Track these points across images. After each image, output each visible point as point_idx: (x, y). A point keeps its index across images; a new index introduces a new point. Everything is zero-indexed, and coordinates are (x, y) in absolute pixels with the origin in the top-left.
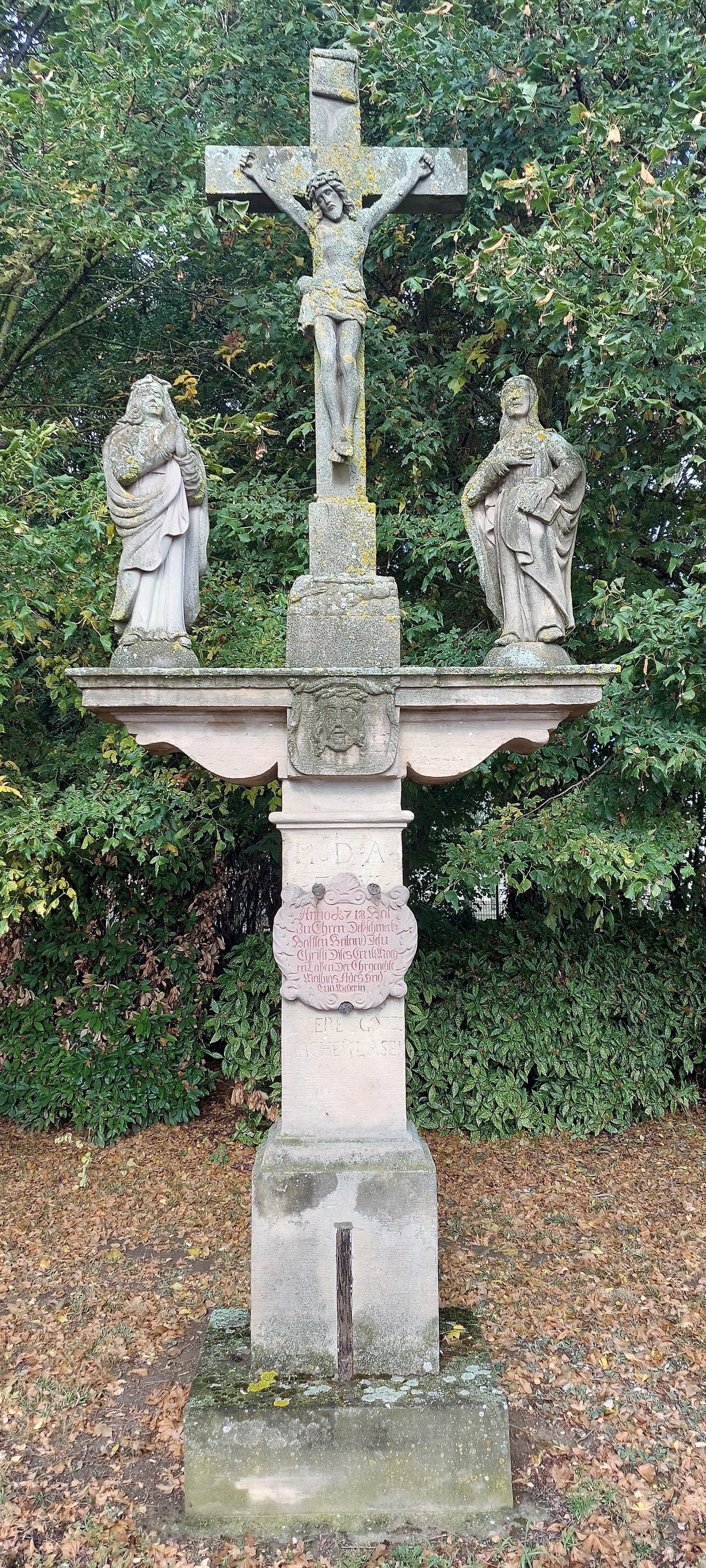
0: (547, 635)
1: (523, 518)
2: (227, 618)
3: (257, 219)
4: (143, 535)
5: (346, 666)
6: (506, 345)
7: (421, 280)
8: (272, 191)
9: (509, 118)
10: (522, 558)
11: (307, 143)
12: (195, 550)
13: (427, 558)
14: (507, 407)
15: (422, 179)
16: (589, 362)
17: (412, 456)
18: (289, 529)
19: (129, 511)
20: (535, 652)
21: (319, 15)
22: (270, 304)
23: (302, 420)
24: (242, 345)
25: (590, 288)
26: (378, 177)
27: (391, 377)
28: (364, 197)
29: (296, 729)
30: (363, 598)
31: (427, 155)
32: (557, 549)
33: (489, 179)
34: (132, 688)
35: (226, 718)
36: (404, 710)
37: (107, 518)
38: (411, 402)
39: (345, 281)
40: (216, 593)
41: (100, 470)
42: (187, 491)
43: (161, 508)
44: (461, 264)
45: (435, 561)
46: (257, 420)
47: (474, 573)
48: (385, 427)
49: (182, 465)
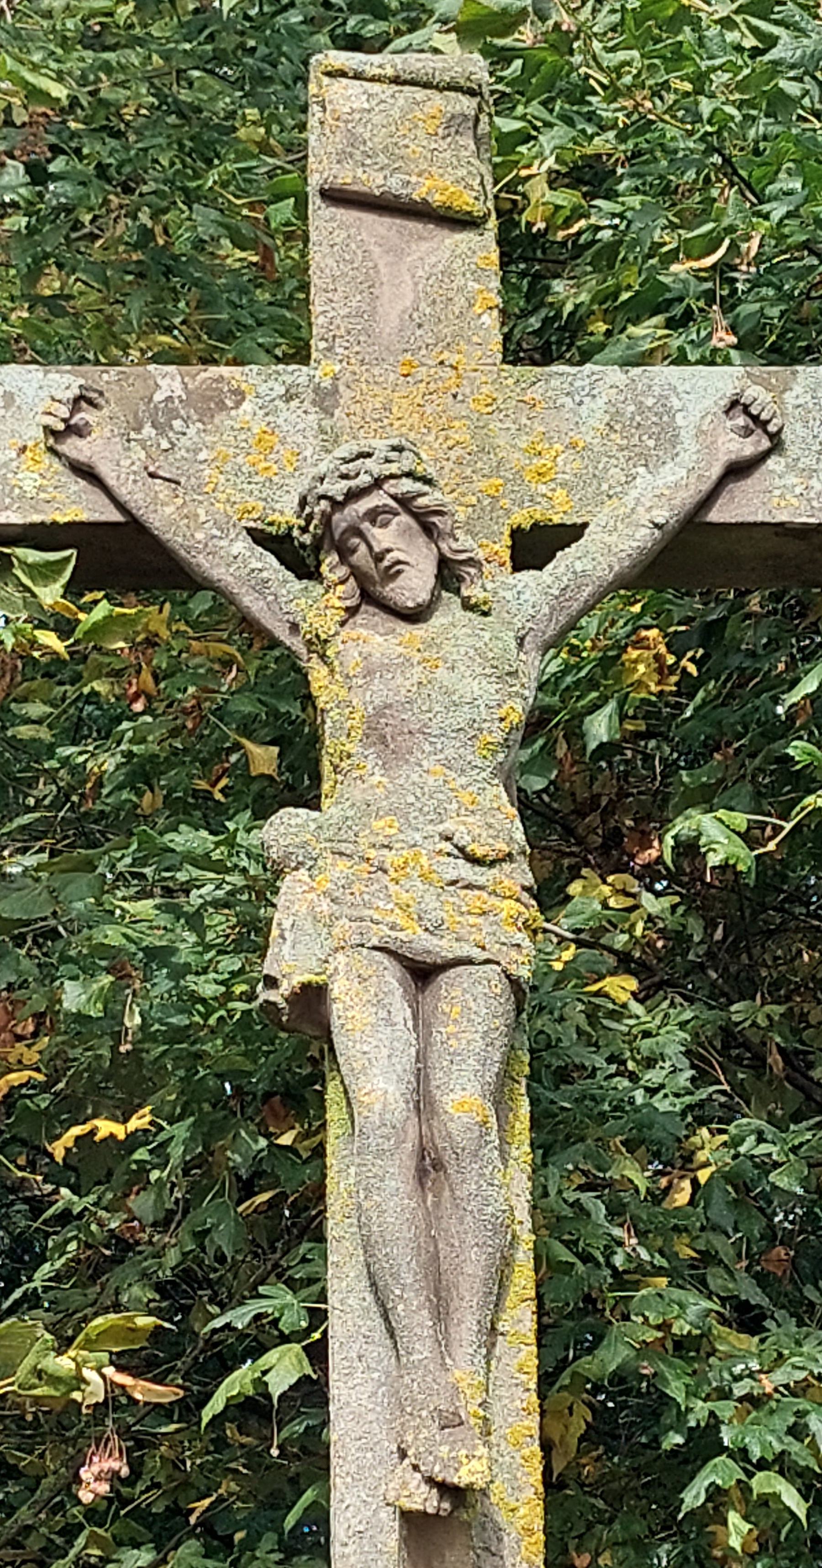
3: (102, 610)
7: (740, 820)
22: (145, 907)
24: (32, 1056)
28: (516, 533)
31: (755, 393)
38: (708, 1258)
39: (449, 826)
46: (89, 1345)
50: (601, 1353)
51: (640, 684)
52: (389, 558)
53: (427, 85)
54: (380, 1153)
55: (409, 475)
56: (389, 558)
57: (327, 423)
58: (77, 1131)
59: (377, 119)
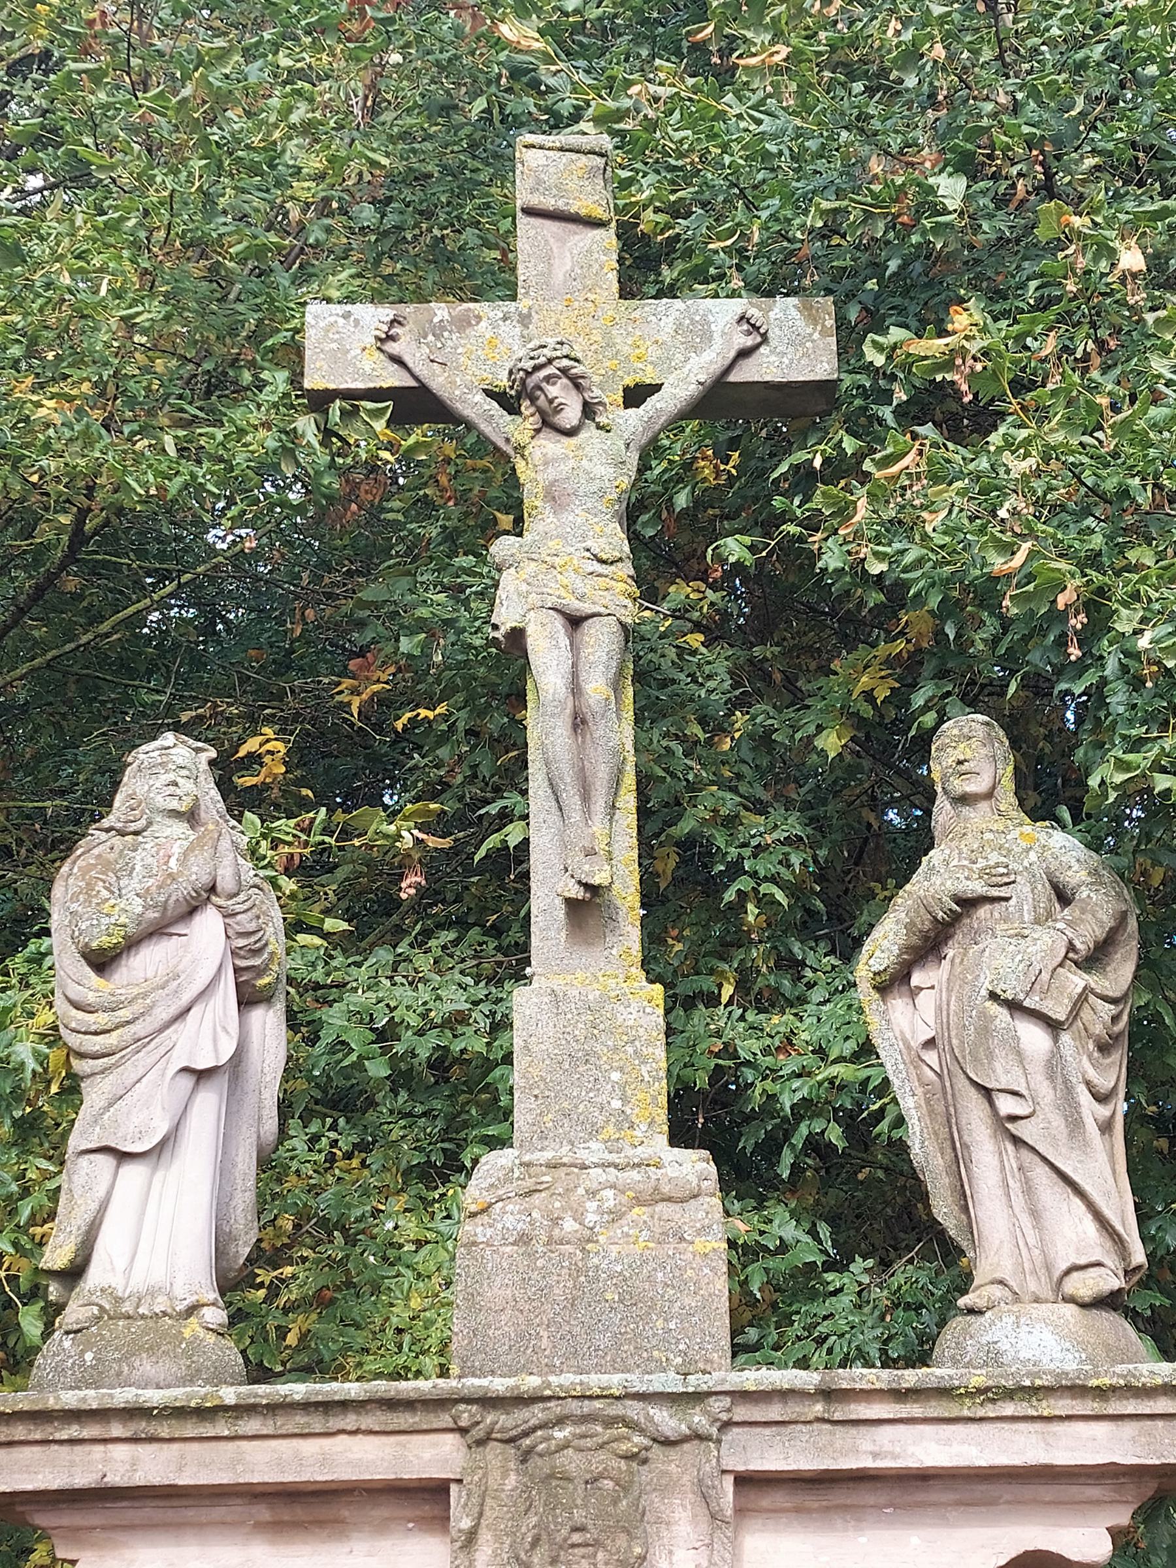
0: (1086, 1285)
1: (1001, 1014)
2: (336, 1249)
4: (129, 1072)
5: (600, 1369)
6: (934, 662)
8: (438, 381)
9: (915, 239)
10: (1006, 1105)
11: (514, 298)
12: (251, 1100)
13: (787, 1102)
14: (945, 779)
15: (744, 354)
16: (1119, 685)
17: (744, 883)
18: (478, 1045)
19: (101, 1019)
20: (1056, 1329)
21: (535, 84)
23: (505, 817)
25: (1109, 538)
26: (654, 353)
27: (695, 730)
28: (626, 390)
29: (471, 1537)
30: (639, 1201)
31: (753, 312)
32: (1088, 1084)
33: (879, 347)
34: (72, 1442)
35: (299, 1512)
36: (744, 1481)
37: (52, 1037)
38: (739, 776)
39: (589, 544)
40: (315, 1190)
41: (47, 932)
42: (237, 970)
43: (173, 1010)
44: (828, 506)
45: (804, 1109)
46: (406, 818)
47: (896, 1134)
48: (685, 826)
49: (228, 915)
50: (680, 824)
51: (705, 480)
52: (557, 402)
53: (578, 152)
54: (553, 715)
55: (567, 357)
56: (557, 402)
57: (525, 332)
58: (409, 715)
59: (552, 170)
